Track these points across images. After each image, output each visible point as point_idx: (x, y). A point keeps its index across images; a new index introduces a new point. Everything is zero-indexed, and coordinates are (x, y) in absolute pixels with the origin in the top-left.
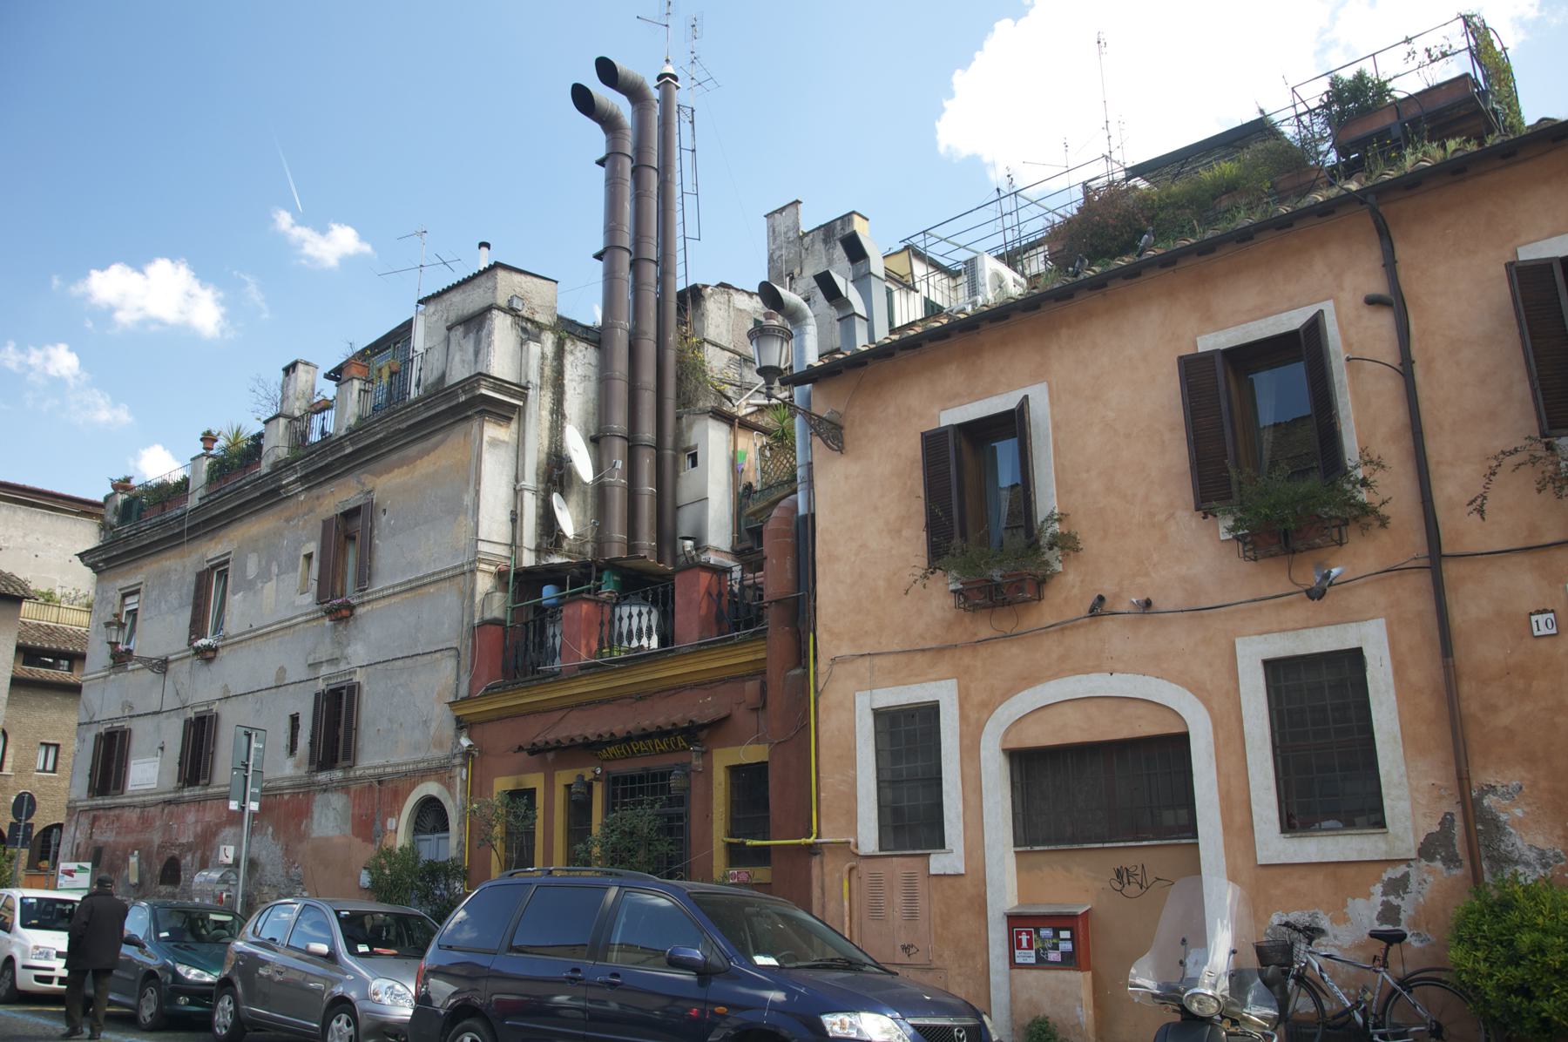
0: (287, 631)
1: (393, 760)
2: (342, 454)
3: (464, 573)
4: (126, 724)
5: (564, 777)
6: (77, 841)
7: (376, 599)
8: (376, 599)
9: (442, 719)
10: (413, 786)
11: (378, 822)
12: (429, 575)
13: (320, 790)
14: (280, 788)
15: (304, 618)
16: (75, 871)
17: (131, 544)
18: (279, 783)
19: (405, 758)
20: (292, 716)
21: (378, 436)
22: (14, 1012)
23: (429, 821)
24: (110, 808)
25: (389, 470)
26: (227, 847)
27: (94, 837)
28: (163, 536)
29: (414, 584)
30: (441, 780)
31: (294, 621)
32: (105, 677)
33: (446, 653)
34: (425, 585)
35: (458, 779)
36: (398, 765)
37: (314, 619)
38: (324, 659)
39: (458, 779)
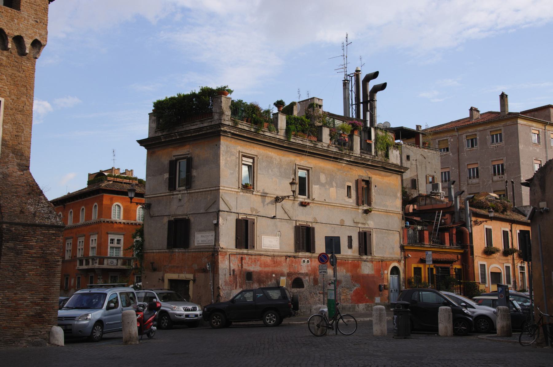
0: (343, 208)
3: (399, 214)
4: (314, 225)
6: (232, 269)
7: (376, 211)
8: (376, 211)
10: (390, 264)
12: (392, 211)
15: (351, 207)
16: (331, 284)
17: (258, 137)
18: (348, 257)
20: (349, 237)
21: (203, 132)
22: (491, 337)
28: (276, 143)
29: (387, 211)
32: (237, 192)
37: (355, 208)
38: (360, 222)
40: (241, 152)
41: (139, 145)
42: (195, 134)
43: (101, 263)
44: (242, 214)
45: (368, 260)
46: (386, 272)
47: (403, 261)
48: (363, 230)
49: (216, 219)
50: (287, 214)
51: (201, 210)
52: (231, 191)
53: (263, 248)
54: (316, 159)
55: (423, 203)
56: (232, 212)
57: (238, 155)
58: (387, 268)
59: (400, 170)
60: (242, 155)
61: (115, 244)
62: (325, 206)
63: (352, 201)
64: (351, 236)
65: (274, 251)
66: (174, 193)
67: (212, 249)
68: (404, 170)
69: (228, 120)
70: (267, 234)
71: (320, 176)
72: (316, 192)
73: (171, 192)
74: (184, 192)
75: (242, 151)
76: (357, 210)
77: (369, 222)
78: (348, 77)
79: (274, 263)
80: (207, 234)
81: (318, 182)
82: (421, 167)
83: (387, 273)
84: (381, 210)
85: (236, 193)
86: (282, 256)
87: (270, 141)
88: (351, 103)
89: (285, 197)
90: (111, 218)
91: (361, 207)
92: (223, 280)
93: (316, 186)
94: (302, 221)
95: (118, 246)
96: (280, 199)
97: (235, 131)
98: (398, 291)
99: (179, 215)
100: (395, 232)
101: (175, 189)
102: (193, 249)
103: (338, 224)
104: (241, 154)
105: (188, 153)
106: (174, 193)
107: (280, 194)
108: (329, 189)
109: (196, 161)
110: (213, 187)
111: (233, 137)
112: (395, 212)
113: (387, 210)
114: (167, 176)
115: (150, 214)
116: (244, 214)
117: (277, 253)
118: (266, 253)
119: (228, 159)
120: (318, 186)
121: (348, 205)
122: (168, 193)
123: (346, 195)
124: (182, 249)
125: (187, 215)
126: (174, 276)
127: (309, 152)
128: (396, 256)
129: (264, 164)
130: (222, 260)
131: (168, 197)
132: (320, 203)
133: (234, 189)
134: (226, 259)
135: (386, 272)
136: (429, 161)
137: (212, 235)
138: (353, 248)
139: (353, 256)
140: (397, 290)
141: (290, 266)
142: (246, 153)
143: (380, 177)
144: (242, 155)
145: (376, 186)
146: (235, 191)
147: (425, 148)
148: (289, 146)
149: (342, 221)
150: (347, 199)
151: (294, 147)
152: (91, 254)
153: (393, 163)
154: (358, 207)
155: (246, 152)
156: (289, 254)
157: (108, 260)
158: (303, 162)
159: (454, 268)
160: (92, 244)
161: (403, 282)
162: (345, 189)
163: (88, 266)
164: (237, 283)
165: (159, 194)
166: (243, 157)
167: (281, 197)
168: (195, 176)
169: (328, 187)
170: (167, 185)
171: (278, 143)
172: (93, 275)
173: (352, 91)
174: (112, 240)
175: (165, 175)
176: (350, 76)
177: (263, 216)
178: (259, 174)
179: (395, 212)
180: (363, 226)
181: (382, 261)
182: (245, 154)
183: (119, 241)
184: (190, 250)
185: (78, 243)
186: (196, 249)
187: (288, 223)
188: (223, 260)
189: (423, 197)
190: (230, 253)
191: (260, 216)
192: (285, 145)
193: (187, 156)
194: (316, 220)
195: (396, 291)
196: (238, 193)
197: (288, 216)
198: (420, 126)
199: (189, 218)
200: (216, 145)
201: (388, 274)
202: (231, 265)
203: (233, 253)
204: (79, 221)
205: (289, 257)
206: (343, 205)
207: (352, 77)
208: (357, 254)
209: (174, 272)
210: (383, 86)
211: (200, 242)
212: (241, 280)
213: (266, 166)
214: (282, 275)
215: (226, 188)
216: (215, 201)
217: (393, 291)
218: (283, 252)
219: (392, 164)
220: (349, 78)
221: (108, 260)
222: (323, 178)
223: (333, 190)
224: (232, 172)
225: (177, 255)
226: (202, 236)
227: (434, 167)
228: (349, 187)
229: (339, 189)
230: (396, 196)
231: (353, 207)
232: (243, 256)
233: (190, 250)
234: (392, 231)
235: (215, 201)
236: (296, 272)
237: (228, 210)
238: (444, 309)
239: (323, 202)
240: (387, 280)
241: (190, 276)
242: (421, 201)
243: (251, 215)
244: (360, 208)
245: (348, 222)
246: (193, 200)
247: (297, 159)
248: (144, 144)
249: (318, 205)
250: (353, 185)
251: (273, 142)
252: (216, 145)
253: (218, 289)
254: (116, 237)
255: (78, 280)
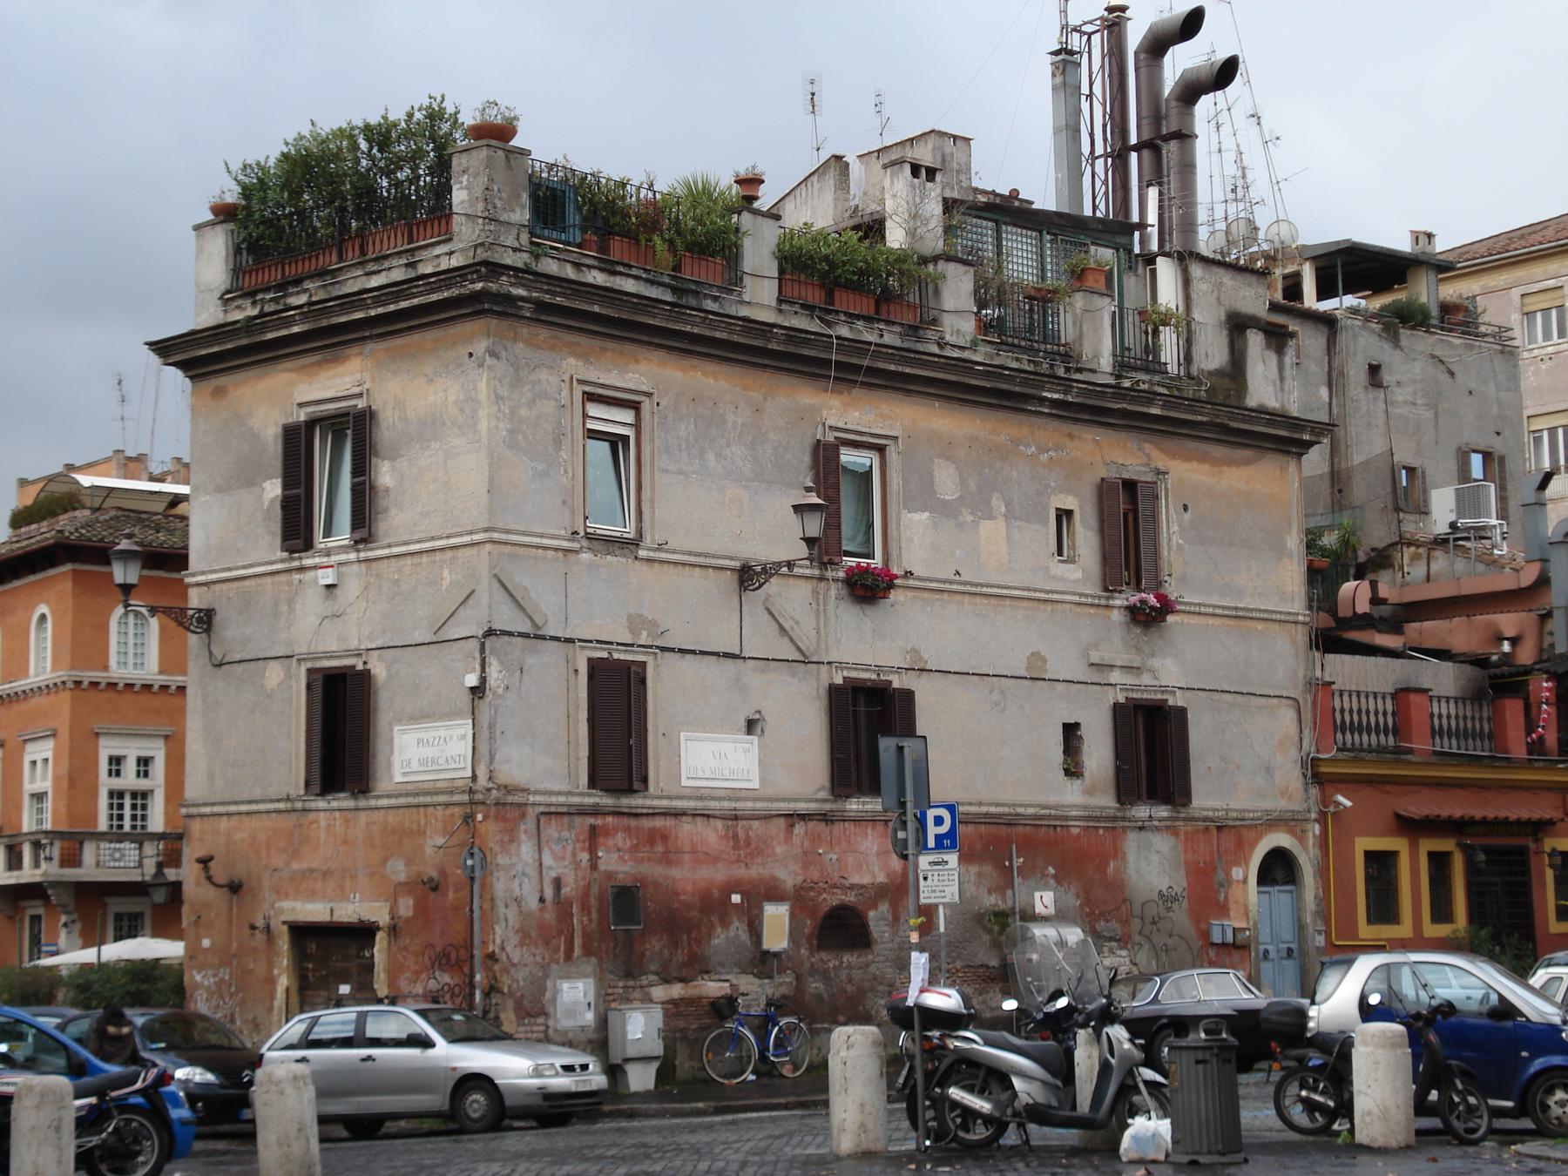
0: (1042, 606)
1: (1233, 805)
2: (1145, 410)
5: (1428, 845)
6: (550, 875)
9: (1289, 774)
11: (1220, 871)
13: (1134, 828)
14: (1067, 818)
15: (1076, 598)
17: (654, 316)
19: (1247, 805)
23: (1279, 874)
24: (637, 815)
25: (1187, 458)
26: (1044, 894)
27: (602, 866)
28: (735, 338)
29: (1241, 614)
30: (1292, 832)
31: (1056, 597)
32: (567, 551)
33: (1284, 701)
34: (1252, 618)
35: (1311, 834)
36: (1244, 811)
37: (1092, 605)
38: (1119, 663)
39: (1311, 834)
40: (580, 382)
41: (155, 359)
42: (380, 310)
43: (71, 859)
44: (591, 641)
45: (1156, 823)
46: (1237, 873)
47: (1317, 828)
48: (1131, 695)
49: (478, 667)
50: (792, 640)
51: (417, 633)
52: (538, 547)
53: (684, 782)
54: (915, 399)
55: (1417, 571)
56: (543, 638)
57: (565, 393)
58: (1241, 857)
59: (1296, 436)
60: (584, 393)
61: (129, 779)
62: (959, 597)
63: (1079, 575)
64: (1076, 726)
65: (734, 794)
66: (308, 562)
67: (463, 792)
68: (1312, 432)
69: (516, 245)
70: (706, 725)
71: (936, 474)
72: (916, 540)
73: (293, 559)
74: (343, 557)
75: (580, 377)
76: (1102, 611)
77: (1156, 663)
78: (1076, 36)
79: (736, 847)
80: (442, 733)
81: (925, 497)
82: (1436, 416)
83: (1241, 877)
84: (1211, 610)
85: (560, 554)
86: (771, 817)
87: (707, 333)
88: (1086, 149)
89: (779, 565)
90: (106, 668)
91: (1119, 601)
92: (510, 925)
93: (916, 516)
94: (857, 666)
95: (143, 784)
96: (758, 574)
97: (547, 292)
98: (1296, 954)
99: (330, 656)
100: (1275, 701)
101: (308, 545)
102: (389, 796)
103: (1018, 674)
104: (578, 391)
105: (357, 390)
106: (308, 562)
107: (761, 552)
108: (975, 524)
109: (388, 428)
110: (461, 535)
111: (543, 318)
112: (1274, 617)
113: (1236, 608)
114: (273, 489)
115: (211, 653)
116: (598, 642)
117: (750, 805)
118: (700, 804)
119: (523, 412)
120: (926, 515)
121: (1062, 593)
122: (282, 561)
123: (1054, 548)
124: (342, 795)
125: (360, 655)
126: (315, 911)
127: (871, 371)
128: (1283, 804)
129: (685, 429)
130: (506, 838)
131: (283, 578)
132: (933, 585)
133: (553, 537)
134: (523, 837)
135: (1237, 873)
136: (1472, 386)
137: (464, 737)
138: (1087, 774)
139: (1086, 808)
140: (1290, 950)
141: (809, 857)
142: (603, 386)
143: (1207, 467)
144: (584, 393)
145: (1185, 508)
146: (556, 550)
147: (1451, 330)
148: (792, 349)
149: (1037, 658)
150: (1059, 569)
151: (813, 353)
152: (28, 824)
153: (1262, 406)
154: (1108, 598)
155: (601, 381)
156: (802, 807)
157: (98, 848)
158: (857, 414)
159: (1547, 849)
160: (32, 781)
161: (1317, 913)
162: (1045, 523)
163: (16, 873)
164: (572, 937)
165: (244, 567)
166: (589, 400)
167: (759, 569)
168: (387, 490)
169: (970, 518)
170: (277, 528)
171: (741, 340)
172: (41, 911)
173: (1090, 96)
174: (116, 762)
175: (267, 485)
176: (1085, 33)
177: (682, 651)
178: (665, 471)
179: (1278, 617)
180: (1130, 680)
181: (1219, 828)
182: (600, 391)
183: (144, 762)
184: (373, 803)
185: (27, 765)
186: (399, 795)
187: (794, 675)
188: (511, 841)
189: (1418, 546)
190: (542, 809)
191: (672, 650)
192: (772, 346)
193: (352, 403)
194: (921, 659)
195: (1284, 954)
196: (571, 557)
197: (793, 648)
198: (1430, 236)
199: (369, 667)
200: (471, 355)
201: (1245, 881)
202: (547, 859)
203: (553, 809)
204: (25, 673)
205: (804, 817)
206: (1040, 591)
207: (1090, 35)
208: (1106, 801)
209: (312, 896)
210: (1226, 72)
211: (415, 766)
212: (590, 920)
213: (691, 438)
214: (775, 895)
215: (514, 538)
216: (473, 592)
217: (1272, 955)
218: (778, 800)
219: (1261, 410)
220: (1076, 42)
221: (98, 848)
222: (946, 481)
223: (992, 531)
224: (541, 467)
225: (323, 823)
226: (420, 741)
227: (1495, 409)
228: (1064, 516)
229: (1018, 523)
230: (1280, 551)
231: (1083, 600)
232: (599, 821)
233: (373, 803)
234: (1264, 700)
235: (473, 592)
236: (836, 880)
237: (526, 627)
238: (1373, 1036)
239: (951, 582)
240: (1242, 910)
241: (378, 913)
242: (1409, 565)
243: (632, 645)
244: (1118, 602)
245: (1066, 663)
246: (385, 589)
247: (832, 402)
248: (178, 358)
249: (927, 595)
250: (1081, 507)
251: (718, 335)
252: (471, 355)
253: (489, 962)
254: (131, 751)
255: (31, 929)
